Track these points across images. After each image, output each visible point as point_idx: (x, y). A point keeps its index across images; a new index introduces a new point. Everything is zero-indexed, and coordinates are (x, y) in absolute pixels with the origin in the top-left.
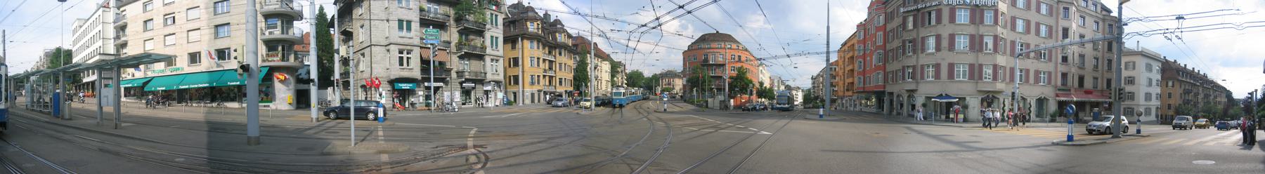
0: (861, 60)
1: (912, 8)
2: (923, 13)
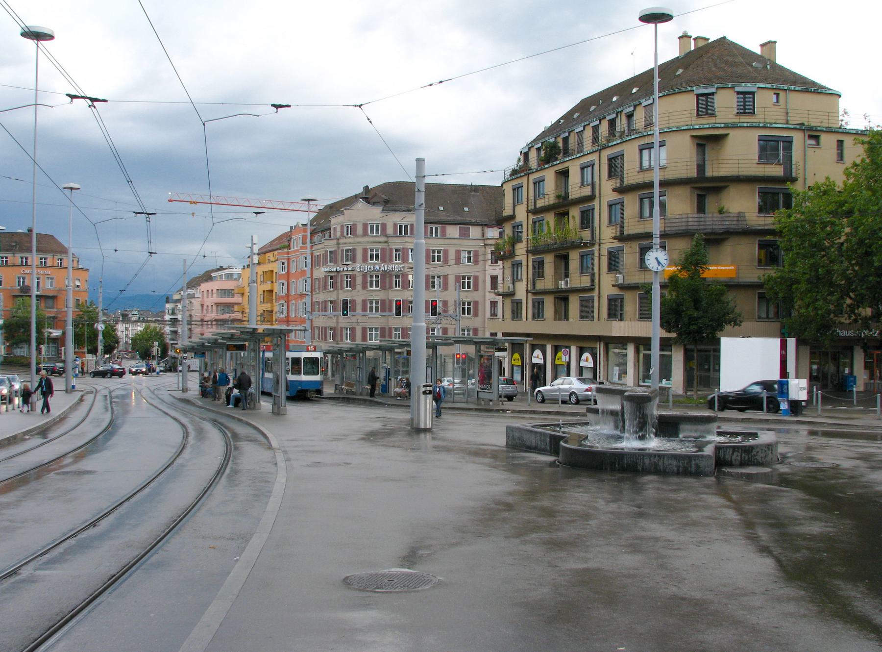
2: (342, 276)
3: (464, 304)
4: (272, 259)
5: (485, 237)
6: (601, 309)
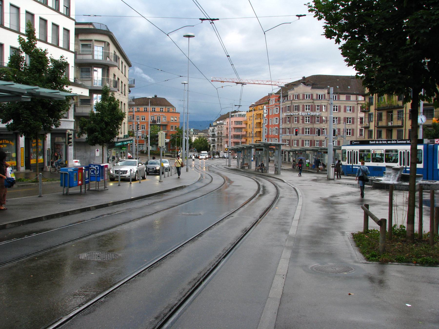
0: (277, 138)
1: (289, 114)
2: (293, 117)
3: (347, 130)
4: (261, 108)
5: (358, 100)
6: (406, 134)
